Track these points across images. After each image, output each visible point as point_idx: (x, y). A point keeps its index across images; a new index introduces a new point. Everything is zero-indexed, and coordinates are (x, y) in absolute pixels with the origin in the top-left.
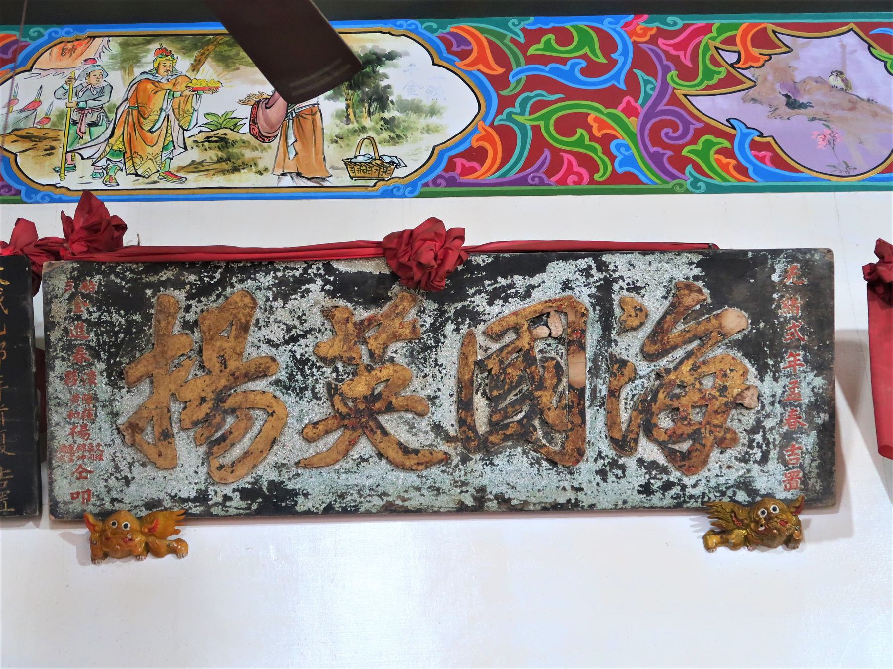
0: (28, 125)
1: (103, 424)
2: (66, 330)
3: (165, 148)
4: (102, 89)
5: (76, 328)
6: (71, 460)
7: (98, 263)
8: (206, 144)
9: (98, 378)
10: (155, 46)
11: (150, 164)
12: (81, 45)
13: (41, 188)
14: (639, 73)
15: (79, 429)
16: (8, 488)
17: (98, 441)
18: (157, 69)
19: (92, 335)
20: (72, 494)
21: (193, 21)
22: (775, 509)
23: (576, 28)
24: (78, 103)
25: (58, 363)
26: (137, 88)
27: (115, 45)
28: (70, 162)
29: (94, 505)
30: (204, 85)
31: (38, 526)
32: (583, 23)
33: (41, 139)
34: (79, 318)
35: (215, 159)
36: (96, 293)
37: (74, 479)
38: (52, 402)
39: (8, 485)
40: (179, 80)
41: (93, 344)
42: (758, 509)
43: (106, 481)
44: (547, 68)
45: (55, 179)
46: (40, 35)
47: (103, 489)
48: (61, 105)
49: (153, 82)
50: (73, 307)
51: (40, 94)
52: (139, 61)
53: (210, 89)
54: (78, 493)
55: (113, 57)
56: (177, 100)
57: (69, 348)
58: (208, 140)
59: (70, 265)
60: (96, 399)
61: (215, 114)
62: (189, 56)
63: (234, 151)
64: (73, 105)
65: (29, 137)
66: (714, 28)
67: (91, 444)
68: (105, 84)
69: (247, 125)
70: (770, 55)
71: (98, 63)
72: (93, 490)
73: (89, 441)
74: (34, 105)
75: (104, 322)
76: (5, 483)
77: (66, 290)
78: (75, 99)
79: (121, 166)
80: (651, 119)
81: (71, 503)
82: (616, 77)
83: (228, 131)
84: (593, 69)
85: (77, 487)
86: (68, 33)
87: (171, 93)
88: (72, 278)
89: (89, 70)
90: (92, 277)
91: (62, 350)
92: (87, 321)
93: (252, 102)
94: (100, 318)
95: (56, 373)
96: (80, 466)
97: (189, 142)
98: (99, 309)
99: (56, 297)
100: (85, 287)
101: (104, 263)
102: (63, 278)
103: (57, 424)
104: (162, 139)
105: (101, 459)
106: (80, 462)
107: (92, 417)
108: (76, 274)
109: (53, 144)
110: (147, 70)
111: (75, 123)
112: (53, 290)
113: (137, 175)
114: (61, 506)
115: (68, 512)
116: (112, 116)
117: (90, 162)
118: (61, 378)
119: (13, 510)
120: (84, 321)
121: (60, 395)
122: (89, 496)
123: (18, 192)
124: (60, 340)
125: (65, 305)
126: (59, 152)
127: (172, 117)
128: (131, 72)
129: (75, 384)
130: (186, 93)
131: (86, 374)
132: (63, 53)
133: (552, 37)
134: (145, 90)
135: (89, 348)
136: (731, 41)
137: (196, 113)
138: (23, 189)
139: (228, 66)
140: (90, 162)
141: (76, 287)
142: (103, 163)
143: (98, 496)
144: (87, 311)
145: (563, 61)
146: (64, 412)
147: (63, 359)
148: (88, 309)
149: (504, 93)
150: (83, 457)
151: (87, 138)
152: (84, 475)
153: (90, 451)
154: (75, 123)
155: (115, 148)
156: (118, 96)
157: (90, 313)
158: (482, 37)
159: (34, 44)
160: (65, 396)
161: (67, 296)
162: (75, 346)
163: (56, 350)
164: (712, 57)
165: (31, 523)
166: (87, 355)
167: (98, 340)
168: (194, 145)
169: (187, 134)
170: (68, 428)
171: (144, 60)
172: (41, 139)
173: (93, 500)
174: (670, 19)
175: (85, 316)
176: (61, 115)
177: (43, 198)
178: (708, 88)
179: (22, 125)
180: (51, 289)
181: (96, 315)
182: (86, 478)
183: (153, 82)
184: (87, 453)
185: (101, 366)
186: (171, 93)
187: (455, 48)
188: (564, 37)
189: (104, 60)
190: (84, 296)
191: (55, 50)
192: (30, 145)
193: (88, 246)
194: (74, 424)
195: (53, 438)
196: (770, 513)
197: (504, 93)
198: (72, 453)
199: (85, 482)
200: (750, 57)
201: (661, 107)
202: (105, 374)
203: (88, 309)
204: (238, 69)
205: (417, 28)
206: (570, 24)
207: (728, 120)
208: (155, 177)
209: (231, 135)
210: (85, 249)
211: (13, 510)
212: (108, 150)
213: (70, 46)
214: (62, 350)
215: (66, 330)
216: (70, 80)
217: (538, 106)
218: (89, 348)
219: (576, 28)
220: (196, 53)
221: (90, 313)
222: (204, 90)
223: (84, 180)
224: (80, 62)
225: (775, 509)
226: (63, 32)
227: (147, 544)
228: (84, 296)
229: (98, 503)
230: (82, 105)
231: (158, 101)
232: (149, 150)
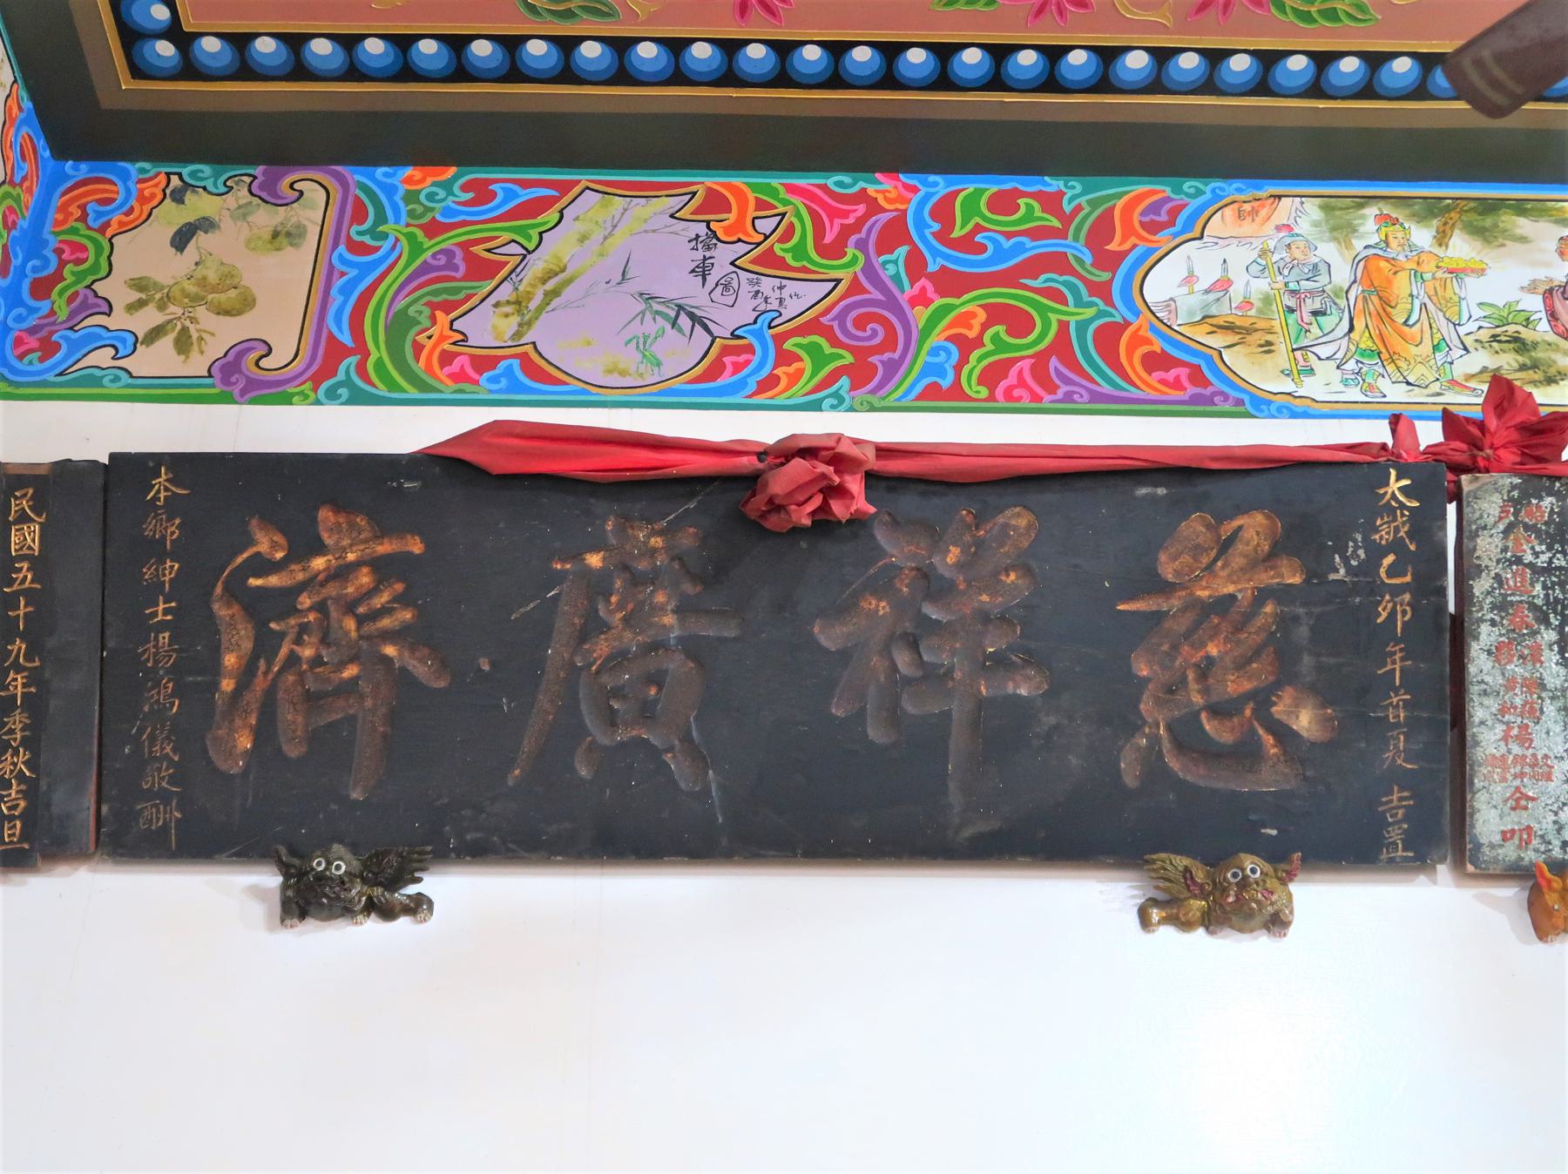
0: (1223, 311)
1: (1550, 724)
2: (1498, 578)
3: (1435, 348)
4: (1315, 266)
5: (1514, 575)
6: (1504, 780)
7: (1550, 477)
8: (1495, 344)
9: (1546, 654)
10: (1372, 211)
11: (1420, 369)
12: (1263, 206)
13: (1271, 397)
15: (1515, 732)
16: (1406, 819)
17: (1545, 751)
18: (1386, 242)
19: (1538, 587)
20: (1504, 833)
21: (1426, 180)
22: (1253, 871)
24: (1286, 284)
25: (1485, 628)
26: (1365, 267)
27: (1312, 209)
28: (1302, 362)
29: (1536, 850)
30: (1462, 265)
31: (1435, 883)
33: (1249, 331)
34: (1518, 560)
35: (1516, 366)
36: (1546, 523)
37: (1506, 809)
38: (1474, 690)
39: (1405, 815)
40: (1423, 257)
41: (1539, 602)
42: (1227, 870)
43: (1556, 814)
45: (1288, 386)
46: (1199, 192)
47: (1551, 826)
48: (1261, 286)
49: (1387, 260)
50: (1510, 544)
51: (1226, 270)
52: (1355, 231)
53: (1473, 271)
54: (1513, 831)
55: (1316, 224)
56: (1430, 285)
57: (1502, 606)
58: (1494, 338)
59: (1508, 480)
60: (1543, 686)
61: (1492, 305)
62: (1427, 227)
63: (1539, 354)
64: (1280, 285)
65: (1229, 328)
67: (1534, 755)
68: (1316, 260)
69: (1545, 320)
71: (1297, 231)
72: (1536, 826)
73: (1531, 751)
74: (1223, 285)
75: (1557, 568)
76: (1401, 812)
77: (1501, 518)
78: (1280, 278)
79: (1381, 370)
81: (1501, 846)
83: (1520, 328)
85: (1513, 821)
86: (1239, 190)
87: (1417, 275)
88: (1511, 499)
89: (1288, 240)
90: (1541, 499)
91: (1492, 609)
92: (1531, 565)
93: (1541, 290)
94: (1550, 561)
95: (1482, 644)
96: (1518, 789)
97: (1469, 341)
98: (1550, 548)
99: (1485, 528)
100: (1528, 514)
101: (1559, 478)
102: (1497, 499)
103: (1482, 723)
104: (1427, 335)
105: (1549, 779)
106: (1517, 783)
107: (1536, 714)
108: (1516, 493)
109: (1269, 337)
110: (1371, 242)
111: (1291, 310)
112: (1481, 517)
113: (1408, 383)
114: (1486, 850)
115: (1496, 861)
116: (1343, 303)
117: (1333, 364)
118: (1489, 653)
119: (1410, 854)
120: (1526, 565)
121: (1487, 678)
122: (1529, 835)
123: (1240, 402)
124: (1488, 593)
125: (1498, 541)
126: (1282, 348)
127: (1430, 306)
128: (1349, 246)
129: (1510, 662)
130: (1439, 274)
131: (1527, 647)
132: (1240, 216)
134: (1379, 270)
135: (1533, 607)
137: (1464, 303)
138: (1246, 398)
139: (1487, 241)
140: (1333, 364)
141: (1516, 514)
142: (1351, 365)
143: (1542, 837)
144: (1535, 552)
146: (1493, 704)
147: (1493, 623)
148: (1533, 548)
150: (1522, 775)
151: (1315, 330)
152: (1523, 803)
153: (1533, 766)
154: (1291, 310)
155: (1362, 346)
156: (1342, 274)
157: (1536, 554)
159: (1195, 203)
160: (1495, 679)
161: (1501, 527)
162: (1512, 604)
163: (1482, 609)
165: (1422, 878)
166: (1530, 618)
167: (1547, 595)
168: (1478, 345)
169: (1462, 330)
170: (1500, 728)
171: (1362, 229)
172: (1249, 331)
173: (1535, 842)
175: (1528, 558)
176: (1267, 300)
177: (1279, 410)
179: (1214, 311)
180: (1477, 515)
181: (1545, 557)
182: (1526, 808)
183: (1387, 260)
184: (1527, 769)
185: (1550, 636)
186: (1417, 275)
189: (1304, 227)
190: (1527, 527)
191: (1228, 211)
192: (1236, 338)
193: (1523, 454)
194: (1507, 723)
195: (1477, 744)
196: (1245, 878)
198: (1505, 769)
199: (1524, 814)
202: (1556, 648)
203: (1533, 548)
204: (1503, 245)
208: (1436, 387)
209: (1526, 334)
210: (1518, 459)
211: (1410, 854)
212: (1353, 348)
213: (1247, 207)
214: (1492, 609)
215: (1498, 578)
216: (1264, 253)
218: (1533, 607)
220: (1435, 222)
221: (1536, 554)
222: (1464, 270)
223: (1333, 388)
224: (1269, 228)
225: (1253, 871)
226: (1232, 188)
227: (370, 898)
228: (1527, 527)
229: (1542, 848)
230: (1293, 286)
231: (1402, 285)
232: (1414, 350)
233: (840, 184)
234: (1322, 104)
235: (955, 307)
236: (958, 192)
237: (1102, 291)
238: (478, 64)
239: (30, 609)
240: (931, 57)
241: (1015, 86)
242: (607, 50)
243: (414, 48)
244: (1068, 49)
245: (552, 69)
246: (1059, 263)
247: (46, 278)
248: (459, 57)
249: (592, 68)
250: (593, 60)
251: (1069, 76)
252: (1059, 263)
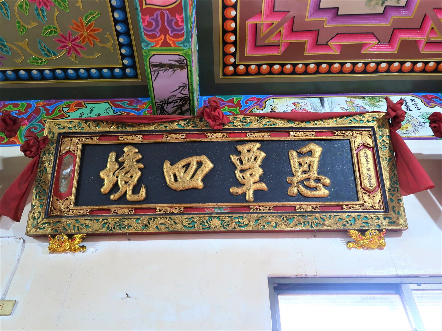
32: (24, 102)
206: (19, 102)
251: (117, 75)
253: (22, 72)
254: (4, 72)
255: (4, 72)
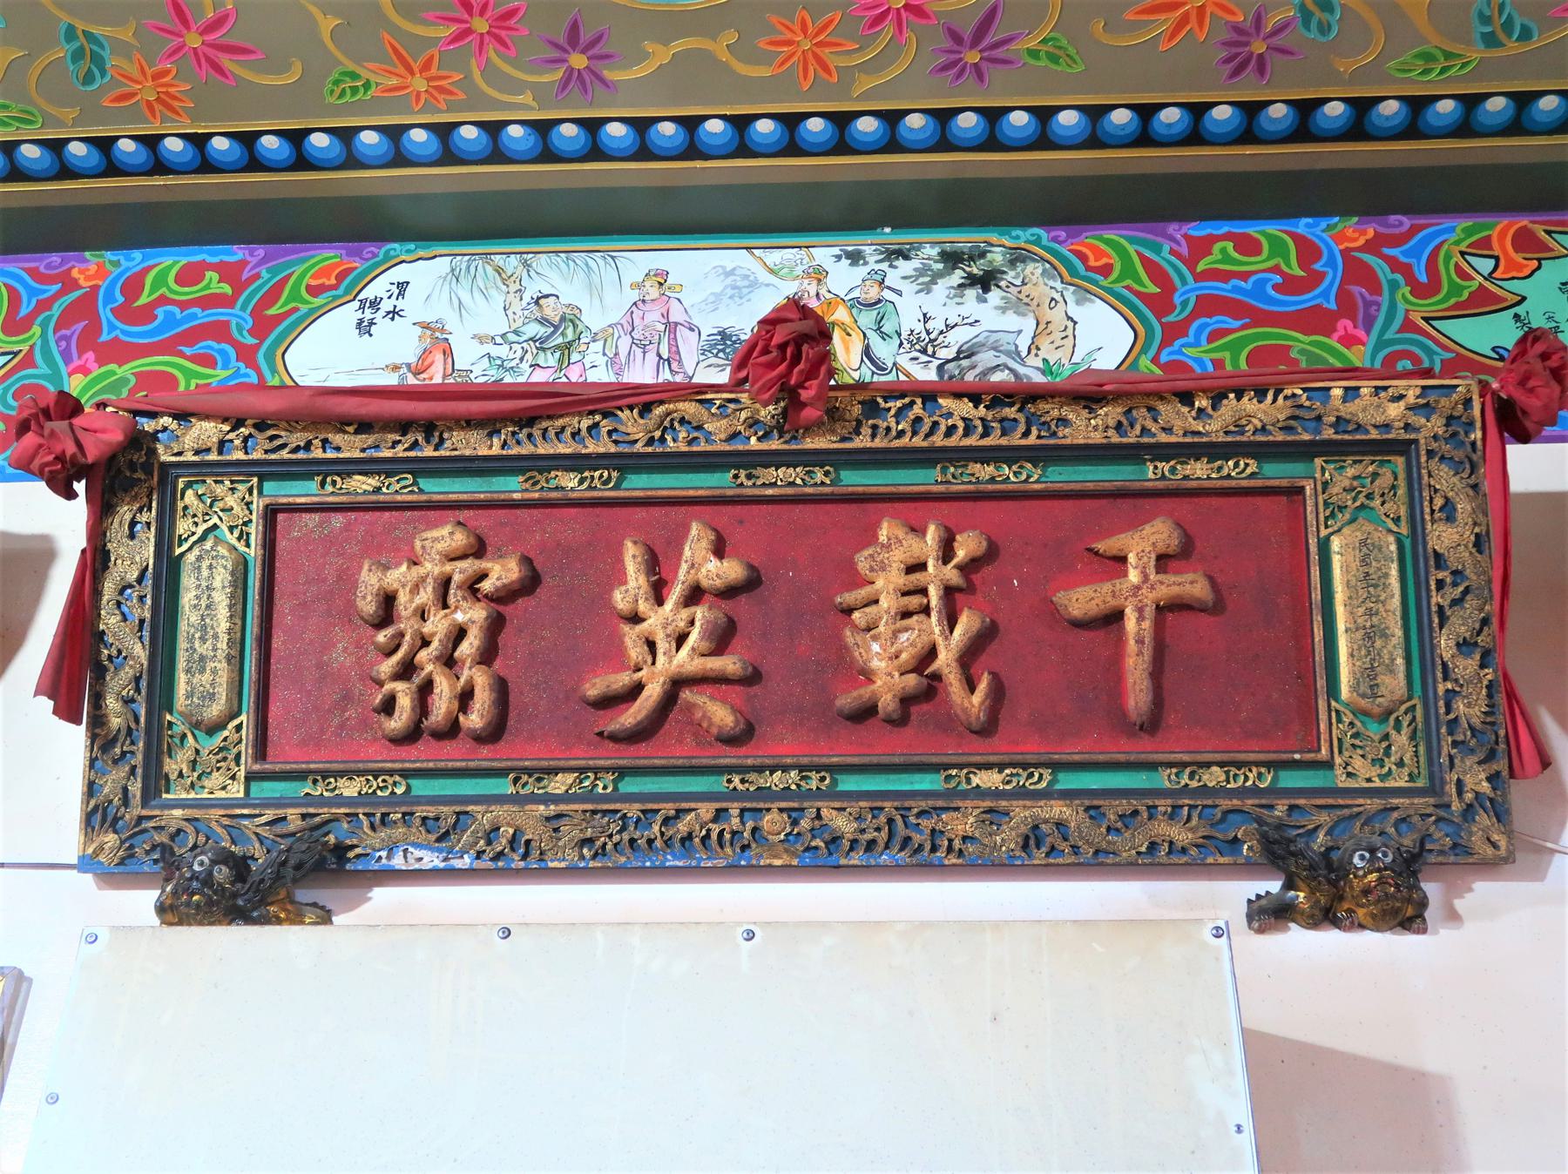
14: (1356, 290)
23: (1263, 233)
32: (1273, 228)
38: (1398, 613)
44: (1228, 286)
46: (375, 255)
66: (1458, 230)
70: (1539, 260)
80: (1200, 238)
82: (1325, 294)
84: (1290, 285)
86: (408, 251)
133: (1230, 245)
136: (1485, 243)
145: (1244, 276)
149: (1171, 318)
158: (1131, 249)
164: (1457, 266)
174: (1393, 218)
178: (1457, 306)
187: (1092, 263)
188: (1248, 246)
197: (1171, 318)
200: (1512, 264)
201: (1389, 335)
205: (1039, 237)
206: (1253, 229)
207: (1493, 349)
217: (1215, 335)
219: (1263, 233)
233: (48, 266)
234: (698, 164)
235: (1208, 325)
236: (150, 268)
237: (247, 355)
238: (269, 156)
239: (1082, 600)
240: (1034, 121)
241: (1109, 141)
242: (1237, 112)
243: (503, 133)
244: (118, 138)
245: (1236, 129)
246: (220, 331)
247: (1199, 316)
248: (742, 137)
249: (614, 146)
250: (468, 140)
252: (220, 331)
253: (319, 140)
254: (10, 148)
255: (10, 148)
